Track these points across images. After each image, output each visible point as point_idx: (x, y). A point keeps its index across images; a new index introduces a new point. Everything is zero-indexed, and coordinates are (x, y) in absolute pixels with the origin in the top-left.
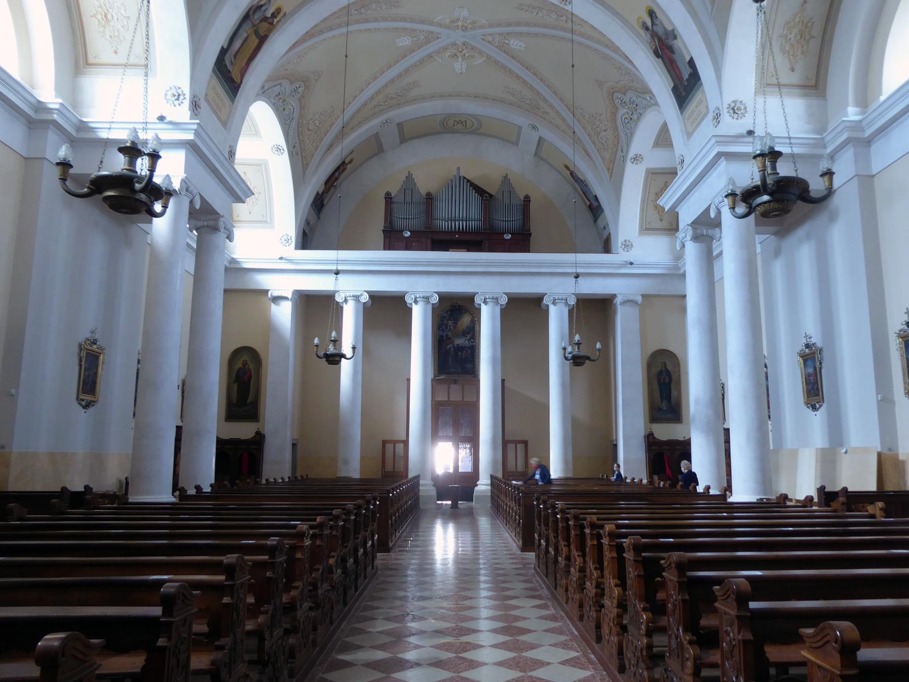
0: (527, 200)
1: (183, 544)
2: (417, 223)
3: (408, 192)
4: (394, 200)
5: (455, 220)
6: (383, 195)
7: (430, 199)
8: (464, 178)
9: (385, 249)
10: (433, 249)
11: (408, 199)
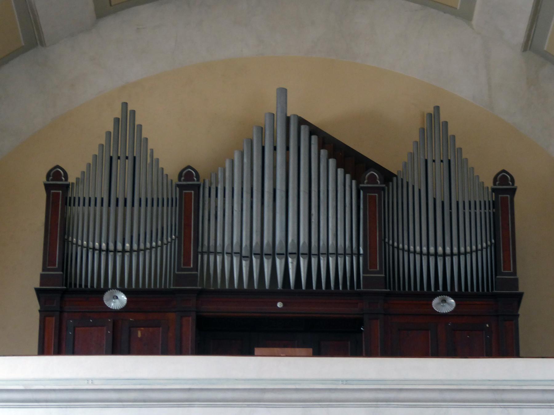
0: (505, 186)
1: (189, 185)
2: (151, 264)
3: (122, 170)
4: (75, 193)
5: (273, 255)
6: (40, 178)
7: (191, 189)
8: (301, 122)
9: (42, 351)
10: (201, 349)
11: (122, 188)
